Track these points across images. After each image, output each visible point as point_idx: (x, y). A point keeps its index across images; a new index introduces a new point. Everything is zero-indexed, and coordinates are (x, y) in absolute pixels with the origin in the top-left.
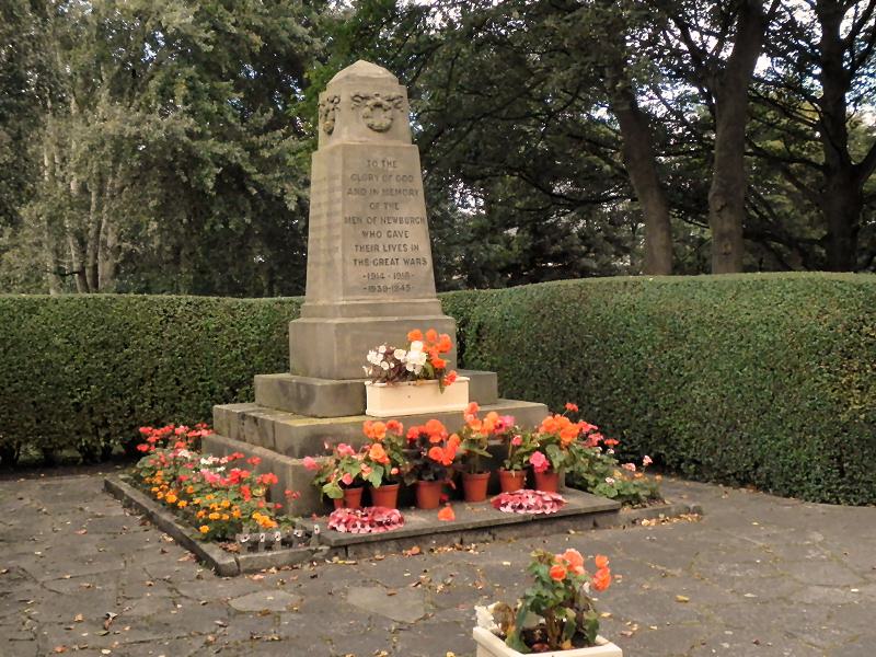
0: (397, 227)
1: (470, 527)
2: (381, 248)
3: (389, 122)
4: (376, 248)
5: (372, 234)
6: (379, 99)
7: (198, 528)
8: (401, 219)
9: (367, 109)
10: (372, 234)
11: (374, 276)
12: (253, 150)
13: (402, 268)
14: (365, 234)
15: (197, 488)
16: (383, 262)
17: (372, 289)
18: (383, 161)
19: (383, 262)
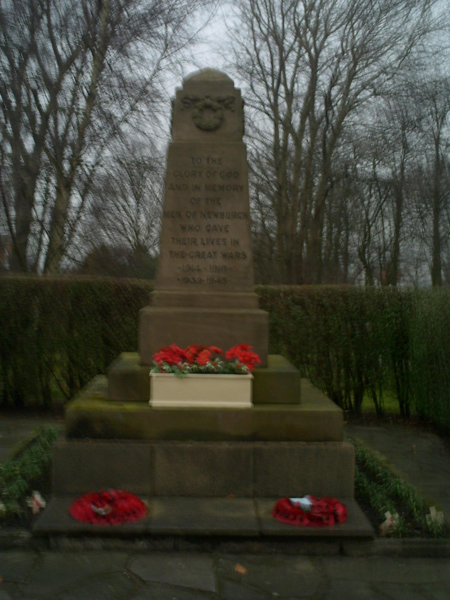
0: (218, 222)
1: (142, 544)
2: (199, 242)
3: (217, 121)
4: (194, 242)
5: (191, 228)
6: (208, 101)
7: (4, 168)
8: (222, 214)
9: (196, 110)
10: (191, 228)
11: (190, 269)
12: (41, 232)
13: (220, 262)
14: (183, 228)
15: (131, 99)
16: (199, 255)
17: (187, 281)
18: (208, 159)
19: (199, 255)
